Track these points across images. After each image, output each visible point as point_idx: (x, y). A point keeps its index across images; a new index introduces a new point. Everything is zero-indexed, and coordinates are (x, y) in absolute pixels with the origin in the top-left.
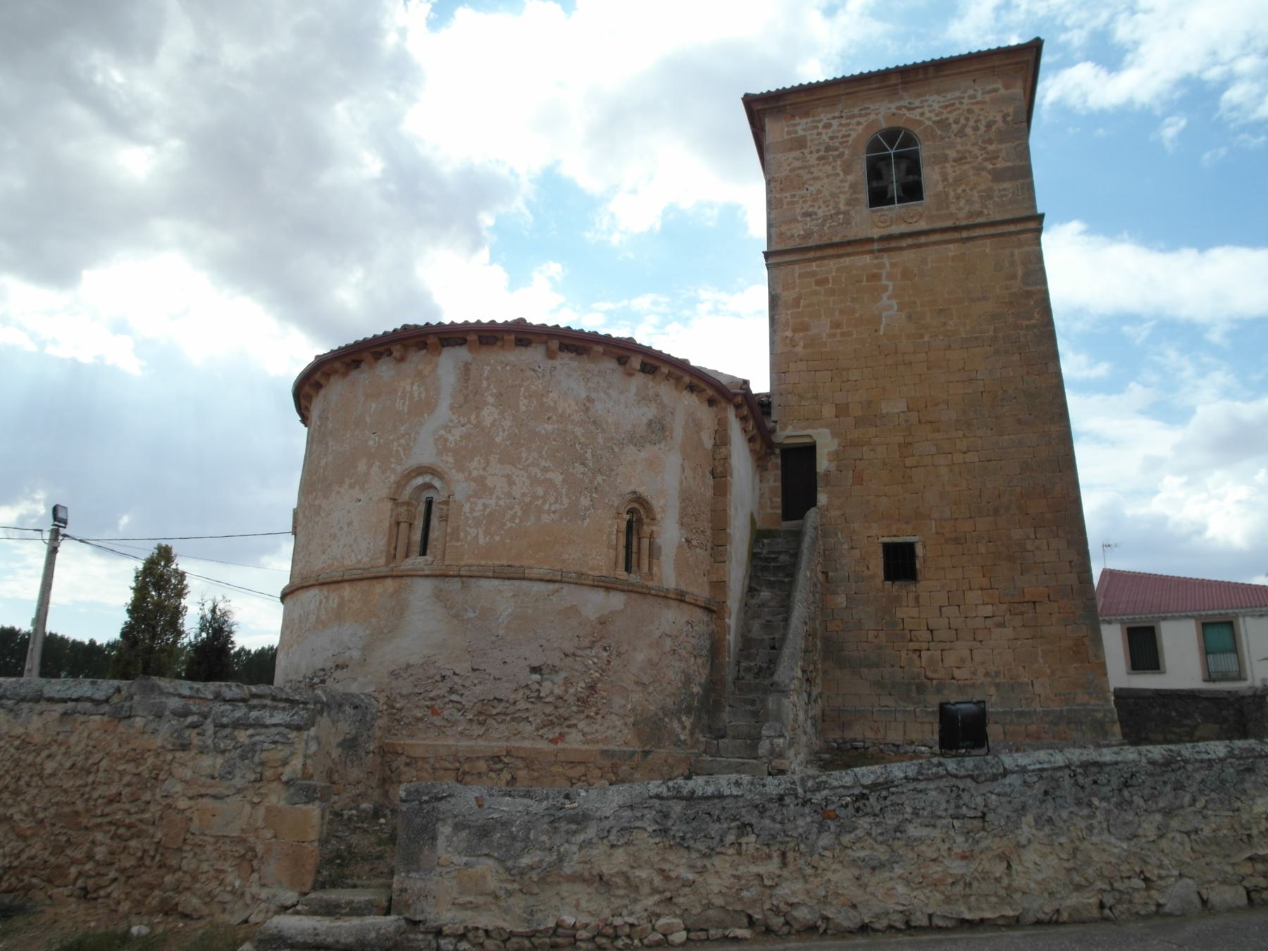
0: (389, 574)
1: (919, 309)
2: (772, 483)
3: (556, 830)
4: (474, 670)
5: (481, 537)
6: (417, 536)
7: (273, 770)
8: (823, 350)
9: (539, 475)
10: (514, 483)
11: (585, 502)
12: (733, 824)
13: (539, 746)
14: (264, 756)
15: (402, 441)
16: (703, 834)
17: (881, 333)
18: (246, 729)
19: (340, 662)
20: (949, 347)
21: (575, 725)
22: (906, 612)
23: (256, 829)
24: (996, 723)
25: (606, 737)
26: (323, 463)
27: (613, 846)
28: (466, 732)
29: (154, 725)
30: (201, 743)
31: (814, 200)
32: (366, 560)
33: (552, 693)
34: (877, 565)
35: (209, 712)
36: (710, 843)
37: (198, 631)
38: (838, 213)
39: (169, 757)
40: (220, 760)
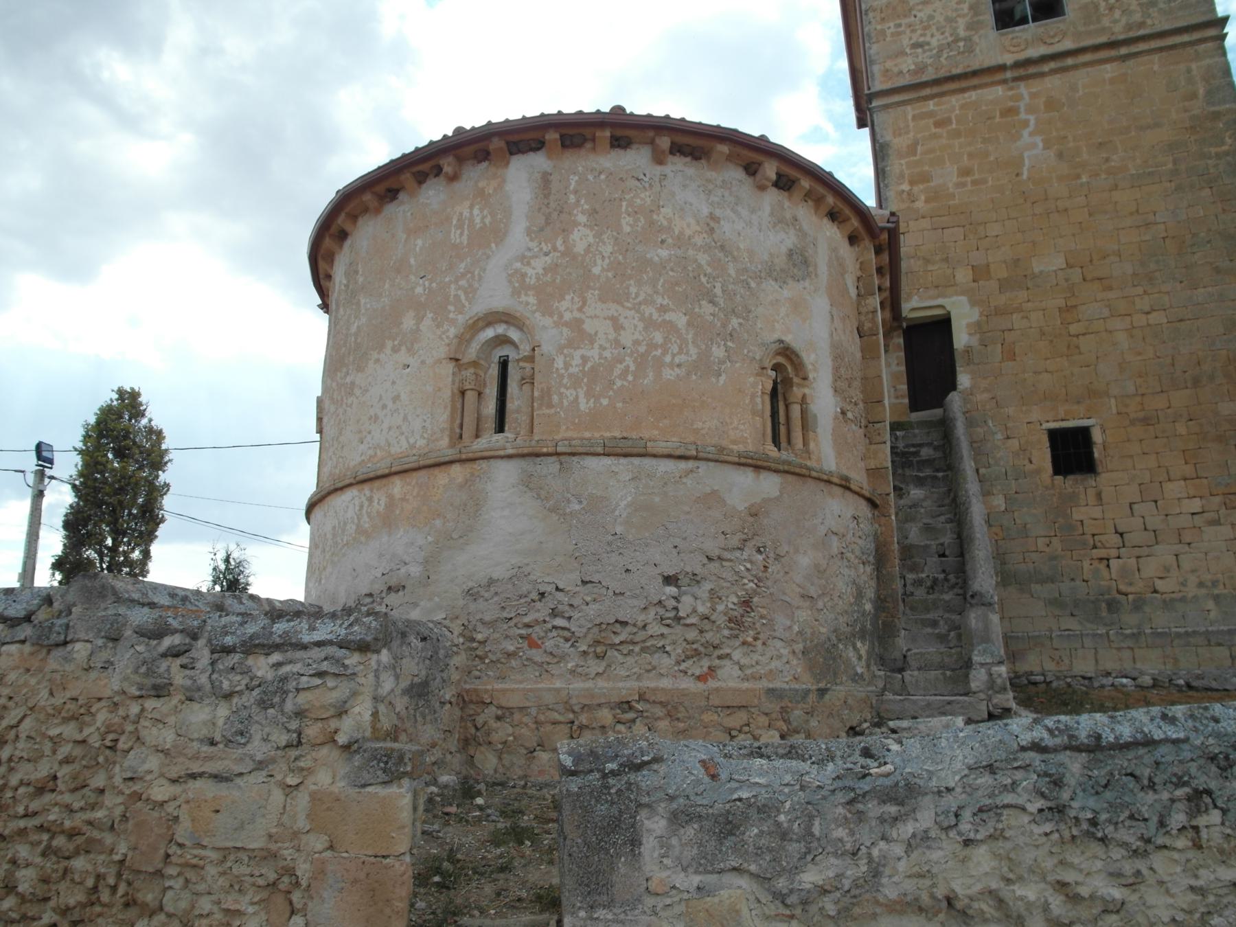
0: (457, 457)
1: (1071, 144)
2: (894, 368)
3: (861, 816)
4: (584, 583)
5: (582, 400)
6: (490, 408)
7: (320, 724)
8: (951, 202)
9: (655, 316)
10: (623, 328)
11: (718, 352)
12: (1180, 792)
13: (683, 686)
14: (302, 699)
15: (463, 283)
16: (1127, 813)
17: (1025, 177)
18: (267, 654)
19: (393, 582)
20: (1116, 187)
21: (728, 656)
22: (1085, 512)
23: (296, 835)
24: (1219, 645)
25: (771, 671)
26: (354, 329)
27: (967, 843)
28: (579, 670)
29: (105, 655)
30: (188, 683)
31: (925, 28)
32: (421, 443)
33: (694, 611)
34: (1043, 457)
35: (201, 628)
36: (1141, 828)
37: (211, 584)
38: (956, 40)
39: (135, 709)
40: (223, 711)
